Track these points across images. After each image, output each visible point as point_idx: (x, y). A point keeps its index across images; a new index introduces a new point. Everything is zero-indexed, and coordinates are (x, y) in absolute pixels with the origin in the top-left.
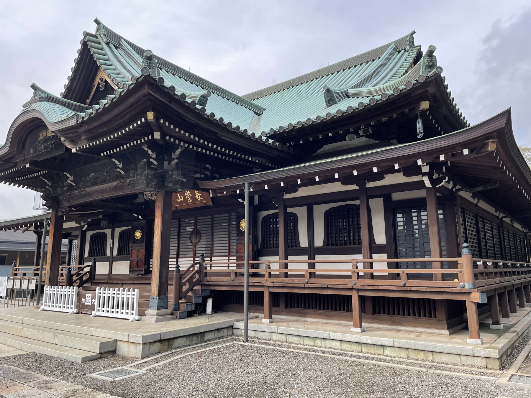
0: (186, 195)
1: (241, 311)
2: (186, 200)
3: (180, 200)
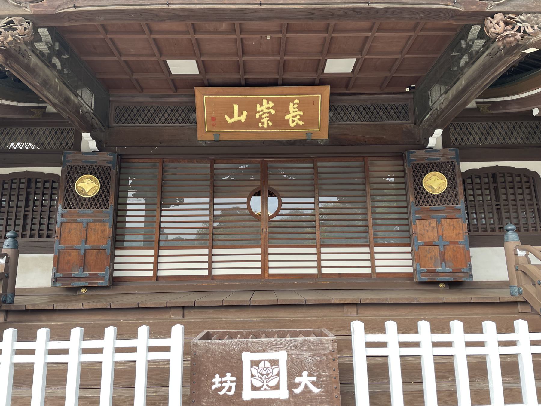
0: (259, 108)
2: (253, 121)
3: (236, 118)
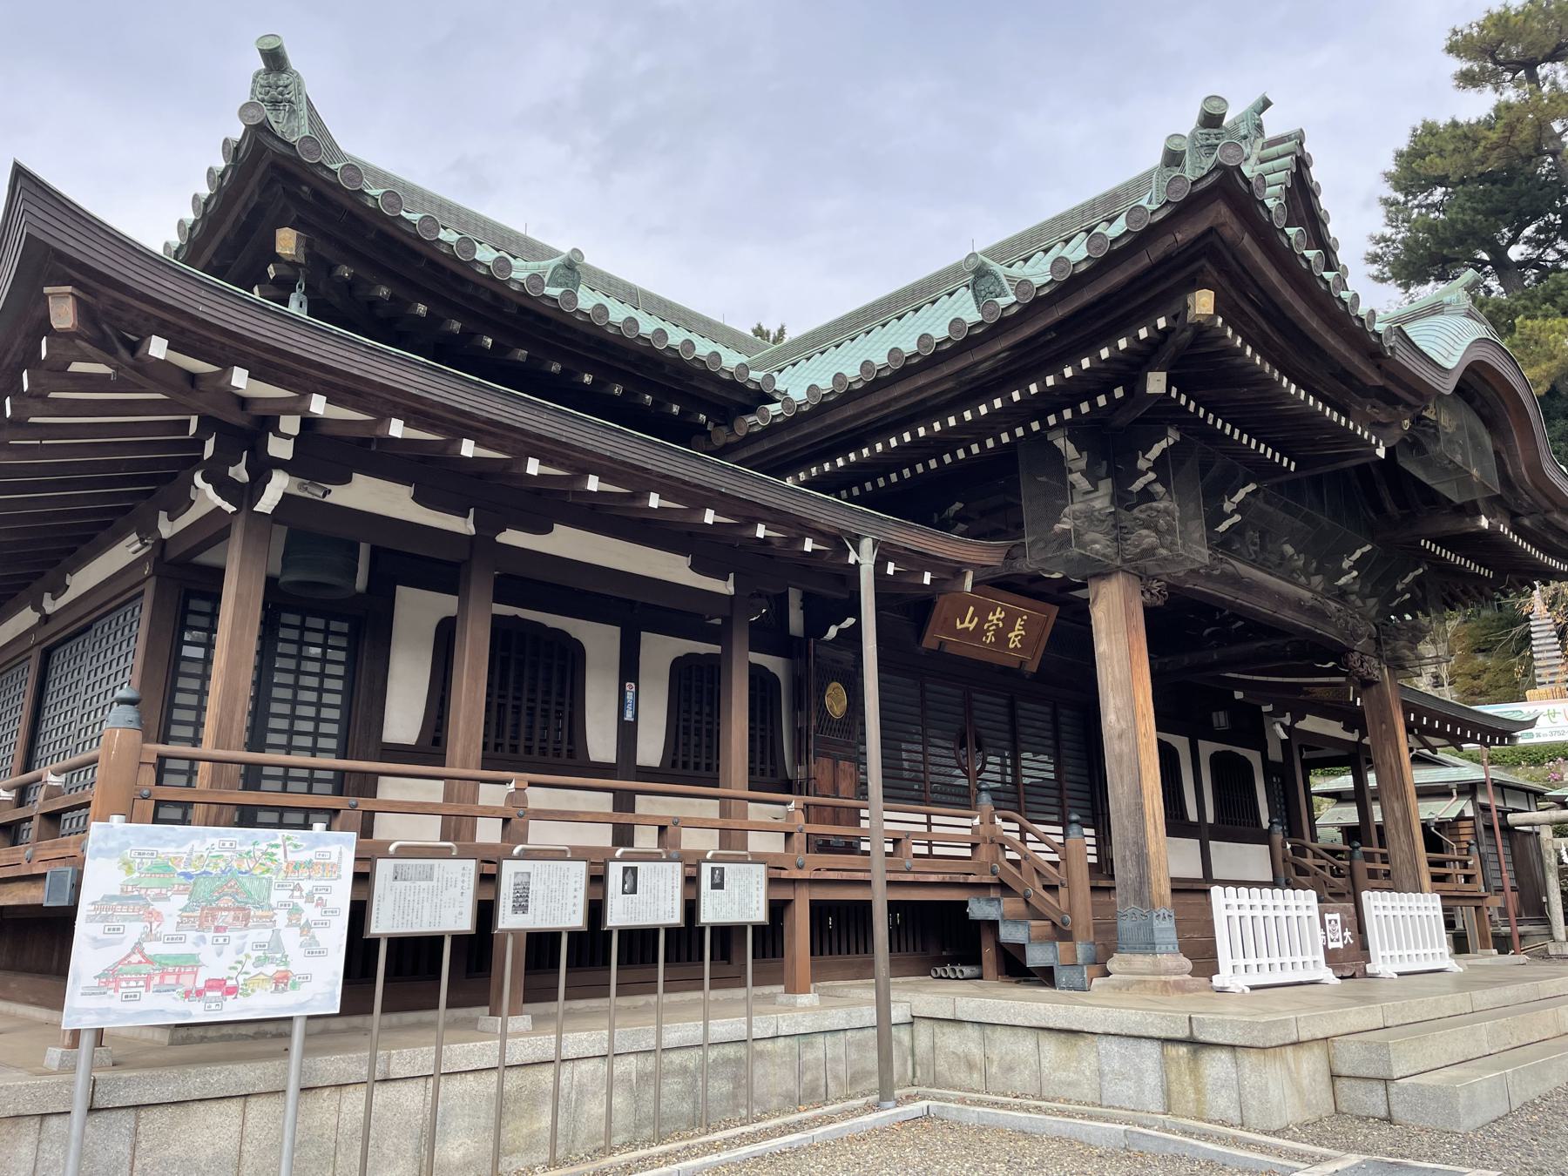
1: (865, 970)
